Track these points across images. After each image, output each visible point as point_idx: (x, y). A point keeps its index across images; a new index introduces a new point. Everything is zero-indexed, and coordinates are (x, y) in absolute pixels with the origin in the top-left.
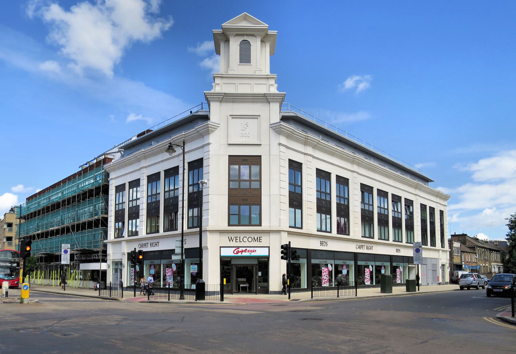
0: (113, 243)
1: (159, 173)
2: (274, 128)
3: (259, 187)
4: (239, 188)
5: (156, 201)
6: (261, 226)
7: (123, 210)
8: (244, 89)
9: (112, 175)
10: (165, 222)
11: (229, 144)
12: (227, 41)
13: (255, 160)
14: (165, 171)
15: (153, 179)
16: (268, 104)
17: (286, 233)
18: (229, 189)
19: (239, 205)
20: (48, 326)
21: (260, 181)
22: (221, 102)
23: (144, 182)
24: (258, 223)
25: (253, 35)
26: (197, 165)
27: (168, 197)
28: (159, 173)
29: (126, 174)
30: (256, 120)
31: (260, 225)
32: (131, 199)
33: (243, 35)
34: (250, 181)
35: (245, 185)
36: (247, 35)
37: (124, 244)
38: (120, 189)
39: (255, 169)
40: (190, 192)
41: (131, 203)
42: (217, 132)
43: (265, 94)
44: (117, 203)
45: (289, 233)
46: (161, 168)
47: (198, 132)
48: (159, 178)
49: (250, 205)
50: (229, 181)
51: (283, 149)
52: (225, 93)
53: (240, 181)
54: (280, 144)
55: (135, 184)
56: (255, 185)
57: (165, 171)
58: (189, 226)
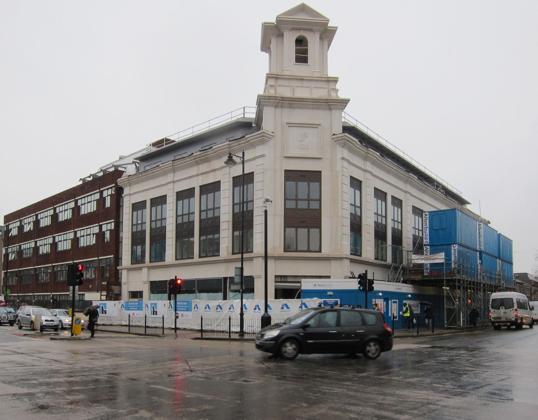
0: (129, 270)
1: (146, 201)
2: (335, 140)
3: (318, 208)
4: (297, 209)
5: (214, 217)
6: (321, 252)
7: (144, 232)
8: (302, 93)
9: (126, 191)
10: (178, 249)
11: (285, 157)
12: (281, 35)
13: (315, 177)
14: (151, 199)
15: (184, 195)
16: (328, 112)
17: (349, 261)
18: (285, 209)
19: (297, 227)
20: (339, 388)
21: (320, 200)
22: (276, 107)
23: (171, 200)
24: (318, 249)
25: (311, 30)
26: (244, 181)
27: (135, 230)
28: (146, 201)
29: (148, 190)
30: (316, 129)
31: (320, 251)
32: (180, 213)
33: (299, 29)
34: (309, 200)
35: (303, 205)
36: (304, 30)
37: (145, 270)
38: (138, 206)
39: (314, 185)
40: (134, 231)
41: (135, 227)
42: (272, 142)
43: (327, 100)
44: (135, 223)
45: (352, 261)
46: (196, 183)
47: (216, 152)
48: (193, 195)
49: (309, 227)
50: (285, 199)
51: (345, 164)
52: (282, 97)
53: (297, 200)
54: (343, 159)
55: (159, 201)
56: (314, 205)
57: (201, 187)
58: (235, 252)
